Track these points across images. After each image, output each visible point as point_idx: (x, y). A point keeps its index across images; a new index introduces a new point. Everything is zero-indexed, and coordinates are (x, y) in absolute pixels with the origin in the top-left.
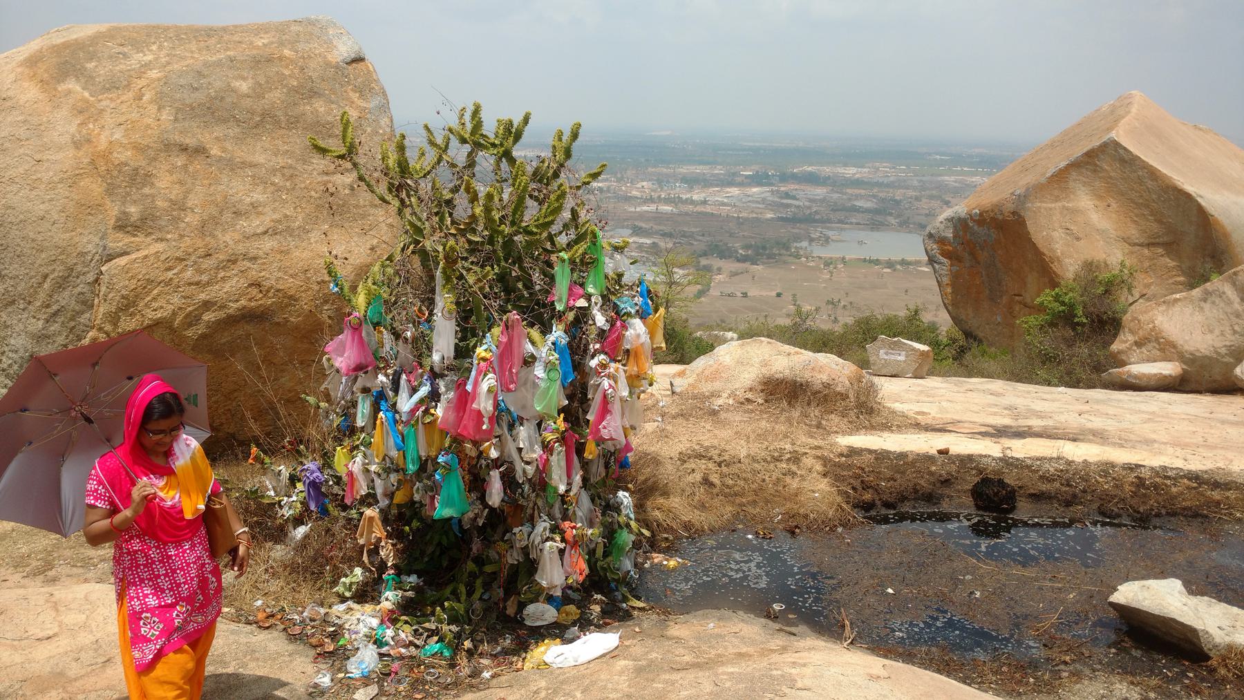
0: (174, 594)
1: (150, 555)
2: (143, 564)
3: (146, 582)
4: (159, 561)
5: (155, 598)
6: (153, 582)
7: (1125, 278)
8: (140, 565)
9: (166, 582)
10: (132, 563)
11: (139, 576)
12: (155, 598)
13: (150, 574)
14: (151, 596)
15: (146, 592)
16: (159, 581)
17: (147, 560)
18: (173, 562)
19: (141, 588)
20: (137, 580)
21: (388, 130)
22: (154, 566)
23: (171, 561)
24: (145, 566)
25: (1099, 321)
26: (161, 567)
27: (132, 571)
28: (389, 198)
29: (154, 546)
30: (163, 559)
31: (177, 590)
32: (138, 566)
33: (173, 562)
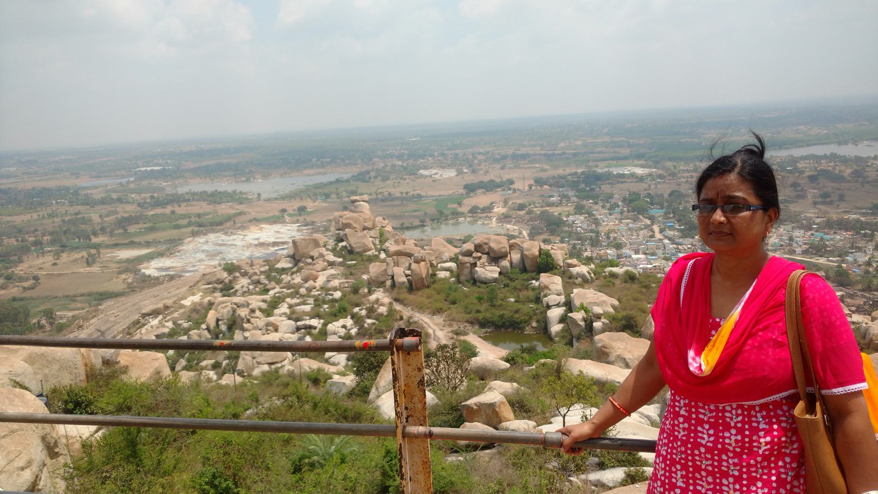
0: (743, 441)
1: (724, 438)
2: (705, 446)
3: (704, 473)
4: (734, 452)
5: (711, 432)
6: (715, 478)
7: (69, 474)
8: (701, 445)
9: (737, 415)
10: (688, 436)
11: (694, 460)
12: (711, 432)
13: (712, 465)
14: (707, 427)
15: (701, 416)
16: (725, 481)
17: (715, 442)
18: (755, 466)
19: (697, 407)
20: (774, 478)
21: (15, 403)
22: (724, 457)
23: (780, 463)
24: (709, 450)
25: (119, 390)
26: (735, 464)
27: (687, 449)
28: (30, 270)
29: (735, 427)
30: (742, 453)
31: (750, 436)
32: (697, 446)
33: (755, 466)
